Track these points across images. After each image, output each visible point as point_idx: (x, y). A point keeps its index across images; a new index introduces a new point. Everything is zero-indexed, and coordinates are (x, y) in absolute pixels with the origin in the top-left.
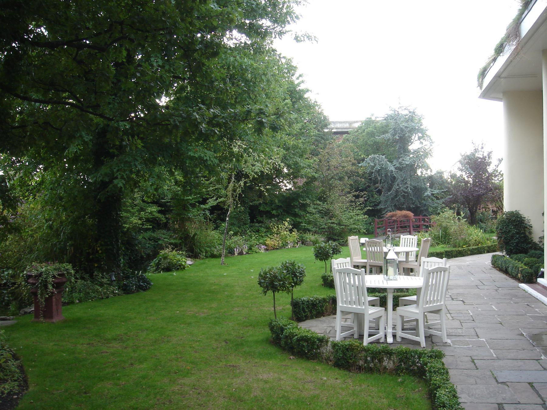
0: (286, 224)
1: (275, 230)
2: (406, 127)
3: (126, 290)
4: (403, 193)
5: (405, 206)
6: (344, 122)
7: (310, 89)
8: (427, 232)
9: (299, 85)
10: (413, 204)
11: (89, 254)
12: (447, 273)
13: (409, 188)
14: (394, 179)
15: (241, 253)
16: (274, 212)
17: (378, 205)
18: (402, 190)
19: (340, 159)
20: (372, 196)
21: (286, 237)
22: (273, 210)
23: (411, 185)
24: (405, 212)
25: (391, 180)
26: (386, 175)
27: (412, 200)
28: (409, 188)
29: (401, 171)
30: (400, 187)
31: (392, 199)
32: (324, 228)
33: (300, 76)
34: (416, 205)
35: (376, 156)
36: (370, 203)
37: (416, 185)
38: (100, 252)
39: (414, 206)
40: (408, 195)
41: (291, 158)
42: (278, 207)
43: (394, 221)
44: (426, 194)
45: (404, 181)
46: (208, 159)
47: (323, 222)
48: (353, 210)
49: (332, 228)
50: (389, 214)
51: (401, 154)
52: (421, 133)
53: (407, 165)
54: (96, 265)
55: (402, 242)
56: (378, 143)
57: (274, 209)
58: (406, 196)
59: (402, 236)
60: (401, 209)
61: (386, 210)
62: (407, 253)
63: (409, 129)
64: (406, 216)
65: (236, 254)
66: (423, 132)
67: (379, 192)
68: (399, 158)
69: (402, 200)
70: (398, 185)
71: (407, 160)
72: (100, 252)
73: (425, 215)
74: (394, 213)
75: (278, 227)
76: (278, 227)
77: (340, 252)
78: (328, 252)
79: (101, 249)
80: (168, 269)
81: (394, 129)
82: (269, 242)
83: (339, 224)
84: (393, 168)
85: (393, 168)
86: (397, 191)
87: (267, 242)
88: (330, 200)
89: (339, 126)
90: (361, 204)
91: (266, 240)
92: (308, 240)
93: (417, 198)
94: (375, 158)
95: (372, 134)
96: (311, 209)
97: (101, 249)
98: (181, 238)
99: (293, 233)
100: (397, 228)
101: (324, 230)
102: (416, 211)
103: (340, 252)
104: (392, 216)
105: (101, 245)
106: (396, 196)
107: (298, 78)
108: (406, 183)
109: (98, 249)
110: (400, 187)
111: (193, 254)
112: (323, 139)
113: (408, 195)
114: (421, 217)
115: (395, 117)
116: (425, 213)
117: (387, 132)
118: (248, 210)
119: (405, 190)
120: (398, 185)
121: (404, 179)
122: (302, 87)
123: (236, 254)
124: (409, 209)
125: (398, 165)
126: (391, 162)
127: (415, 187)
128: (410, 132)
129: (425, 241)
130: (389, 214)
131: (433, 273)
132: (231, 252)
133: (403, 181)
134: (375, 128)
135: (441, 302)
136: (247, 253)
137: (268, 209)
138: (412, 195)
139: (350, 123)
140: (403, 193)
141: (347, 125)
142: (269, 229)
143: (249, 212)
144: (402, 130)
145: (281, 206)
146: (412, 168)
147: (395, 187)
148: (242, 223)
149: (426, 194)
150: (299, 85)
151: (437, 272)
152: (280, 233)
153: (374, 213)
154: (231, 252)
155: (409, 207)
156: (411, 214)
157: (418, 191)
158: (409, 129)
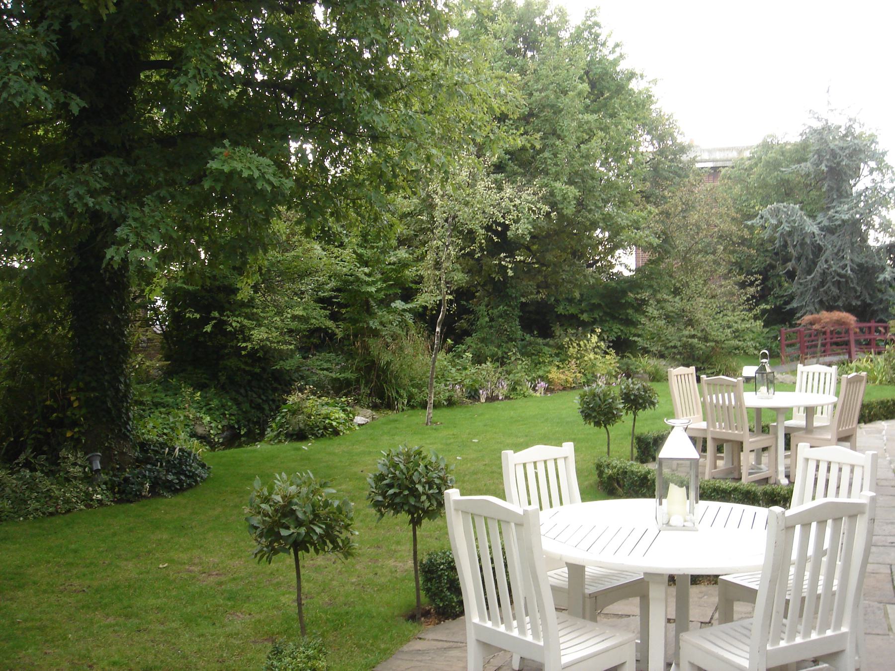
0: (595, 339)
1: (572, 351)
2: (842, 149)
3: (124, 494)
4: (837, 278)
5: (840, 303)
6: (728, 149)
7: (638, 72)
8: (879, 353)
9: (615, 63)
10: (857, 298)
11: (51, 409)
12: (861, 524)
13: (848, 268)
14: (818, 250)
15: (492, 399)
16: (585, 317)
17: (787, 303)
18: (835, 271)
19: (711, 215)
20: (780, 286)
21: (594, 365)
22: (582, 312)
23: (852, 260)
24: (837, 315)
25: (813, 253)
26: (803, 244)
27: (856, 291)
28: (848, 268)
29: (834, 234)
30: (830, 266)
31: (816, 289)
32: (675, 347)
33: (617, 45)
34: (864, 301)
35: (781, 205)
36: (776, 298)
37: (863, 261)
38: (76, 404)
39: (859, 303)
40: (847, 282)
41: (597, 207)
42: (593, 308)
43: (818, 333)
44: (881, 277)
45: (838, 255)
46: (257, 174)
47: (673, 335)
48: (733, 311)
49: (692, 347)
50: (808, 318)
51: (833, 200)
52: (872, 158)
53: (843, 221)
54: (69, 434)
55: (800, 379)
56: (788, 181)
57: (586, 311)
58: (842, 283)
59: (800, 367)
60: (830, 309)
61: (803, 312)
62: (810, 411)
63: (847, 151)
64: (840, 323)
65: (483, 400)
66: (879, 158)
67: (791, 275)
68: (829, 209)
69: (835, 291)
70: (826, 261)
71: (843, 212)
72: (76, 404)
73: (881, 321)
74: (816, 316)
75: (579, 345)
76: (579, 345)
77: (653, 404)
78: (610, 407)
79: (77, 399)
80: (300, 436)
81: (818, 152)
82: (554, 374)
83: (706, 339)
84: (815, 229)
85: (815, 229)
86: (824, 273)
87: (550, 376)
88: (687, 292)
89: (718, 156)
90: (748, 300)
91: (549, 372)
92: (640, 370)
93: (865, 287)
94: (778, 210)
95: (775, 165)
96: (652, 311)
97: (77, 399)
98: (358, 370)
99: (608, 357)
100: (823, 345)
101: (675, 350)
102: (863, 313)
103: (653, 404)
104: (812, 323)
105: (79, 390)
106: (823, 284)
107: (613, 51)
108: (843, 257)
109: (73, 398)
110: (830, 266)
111: (383, 401)
112: (679, 176)
113: (847, 282)
114: (873, 324)
115: (822, 134)
116: (882, 317)
117: (806, 160)
118: (517, 312)
119: (840, 271)
120: (826, 261)
121: (839, 250)
122: (623, 66)
123: (483, 400)
124: (849, 309)
125: (826, 223)
126: (813, 216)
127: (860, 265)
128: (850, 156)
129: (850, 381)
130: (808, 318)
131: (806, 526)
132: (473, 396)
133: (836, 254)
134: (783, 154)
135: (838, 625)
136: (507, 397)
137: (572, 310)
138: (855, 282)
139: (740, 151)
140: (837, 278)
141: (734, 155)
142: (561, 352)
143: (520, 317)
144: (834, 154)
145: (599, 305)
146: (854, 230)
147: (821, 265)
148: (504, 338)
149: (881, 277)
150: (615, 63)
151: (822, 523)
152: (583, 356)
153: (780, 316)
154: (473, 396)
155: (850, 304)
156: (851, 318)
157: (867, 272)
158: (847, 151)
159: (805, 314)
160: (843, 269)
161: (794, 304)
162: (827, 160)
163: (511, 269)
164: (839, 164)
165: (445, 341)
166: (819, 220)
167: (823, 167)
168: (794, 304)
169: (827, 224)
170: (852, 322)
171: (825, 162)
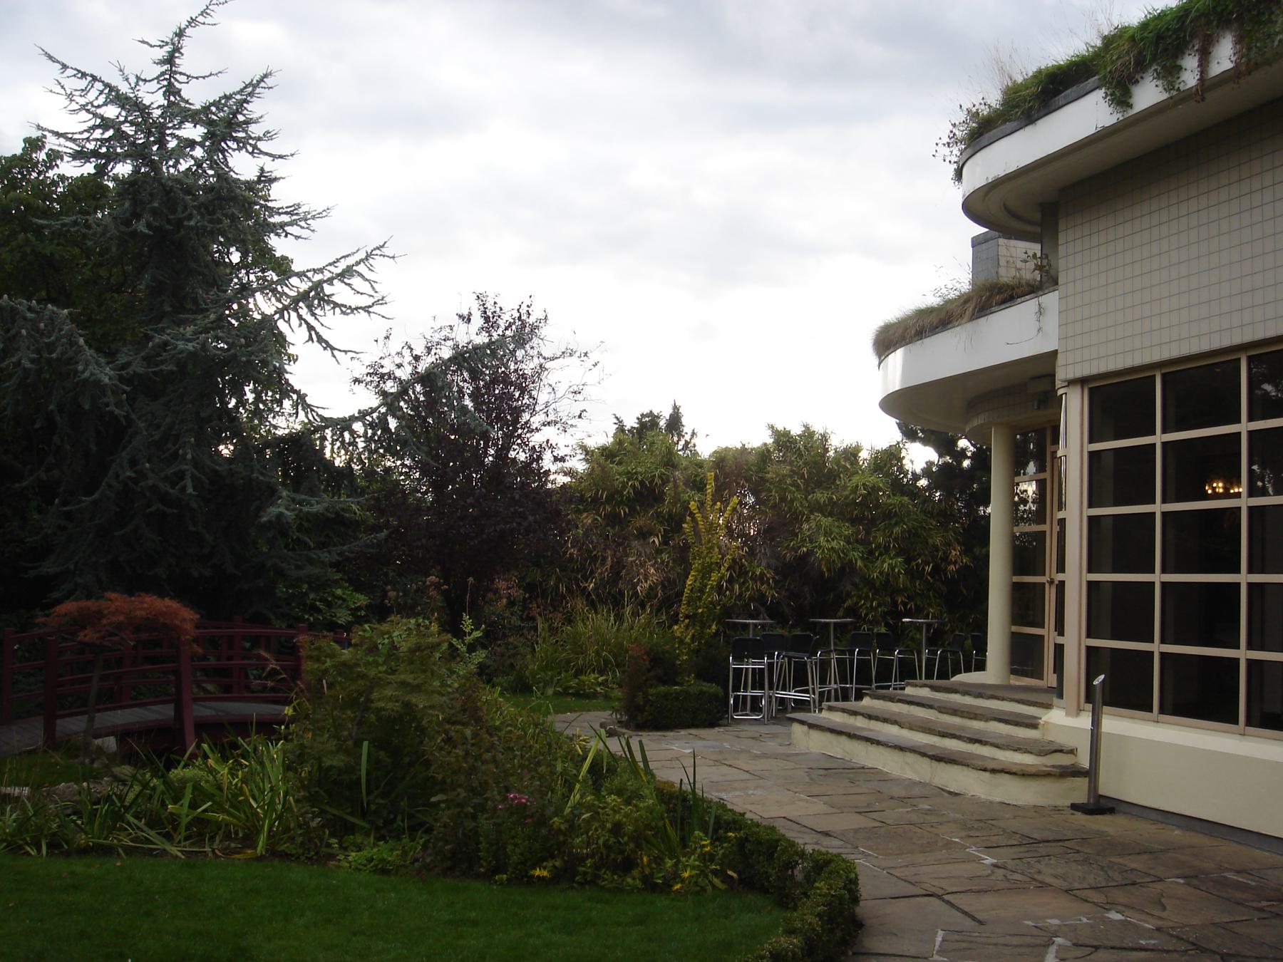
60: (133, 586)
70: (133, 463)
74: (91, 604)
84: (106, 375)
104: (84, 620)
119: (165, 487)
125: (138, 367)
126: (105, 347)
156: (185, 616)
159: (69, 595)
160: (173, 485)
161: (48, 567)
162: (154, 212)
163: (1205, 57)
164: (179, 224)
165: (715, 504)
166: (122, 359)
167: (141, 227)
168: (48, 567)
169: (141, 370)
170: (188, 626)
171: (147, 217)
